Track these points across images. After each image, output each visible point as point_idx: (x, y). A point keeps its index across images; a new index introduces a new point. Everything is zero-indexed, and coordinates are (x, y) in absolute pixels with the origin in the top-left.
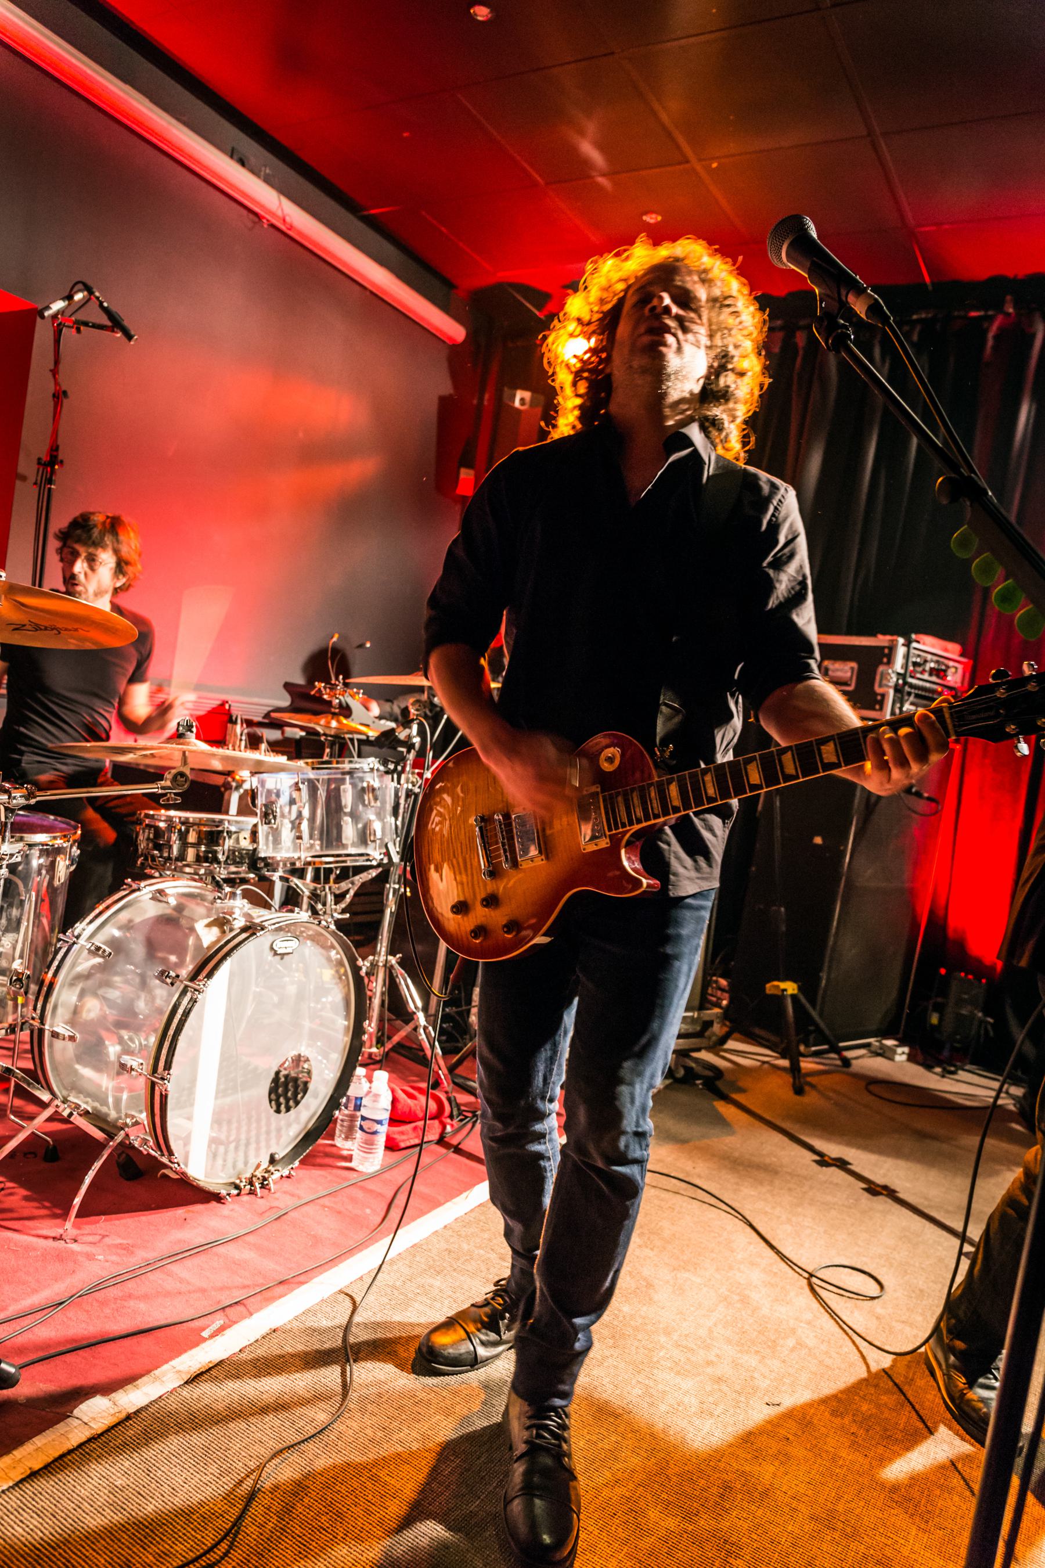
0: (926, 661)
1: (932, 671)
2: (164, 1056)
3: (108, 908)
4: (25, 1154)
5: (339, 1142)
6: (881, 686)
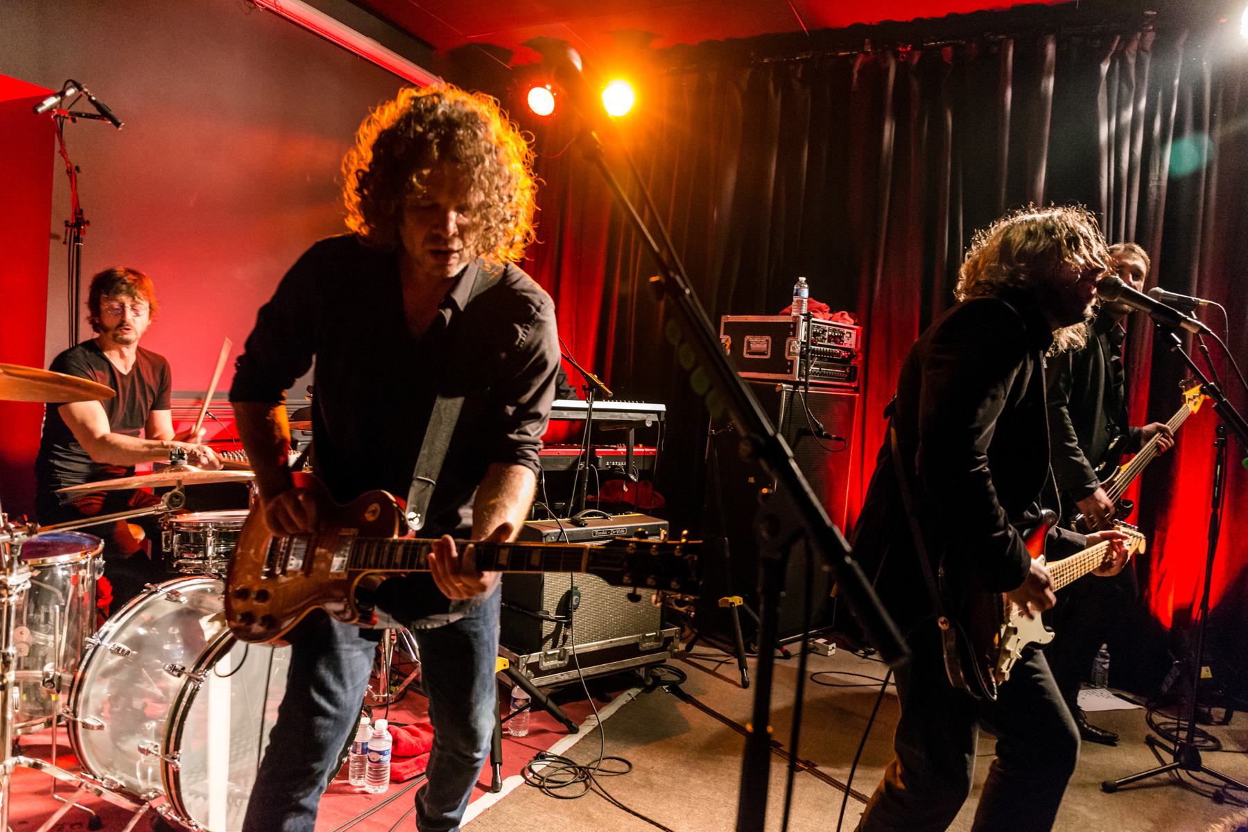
0: (824, 331)
1: (830, 338)
2: (173, 737)
3: (135, 605)
4: (72, 826)
5: (352, 781)
6: (790, 354)
